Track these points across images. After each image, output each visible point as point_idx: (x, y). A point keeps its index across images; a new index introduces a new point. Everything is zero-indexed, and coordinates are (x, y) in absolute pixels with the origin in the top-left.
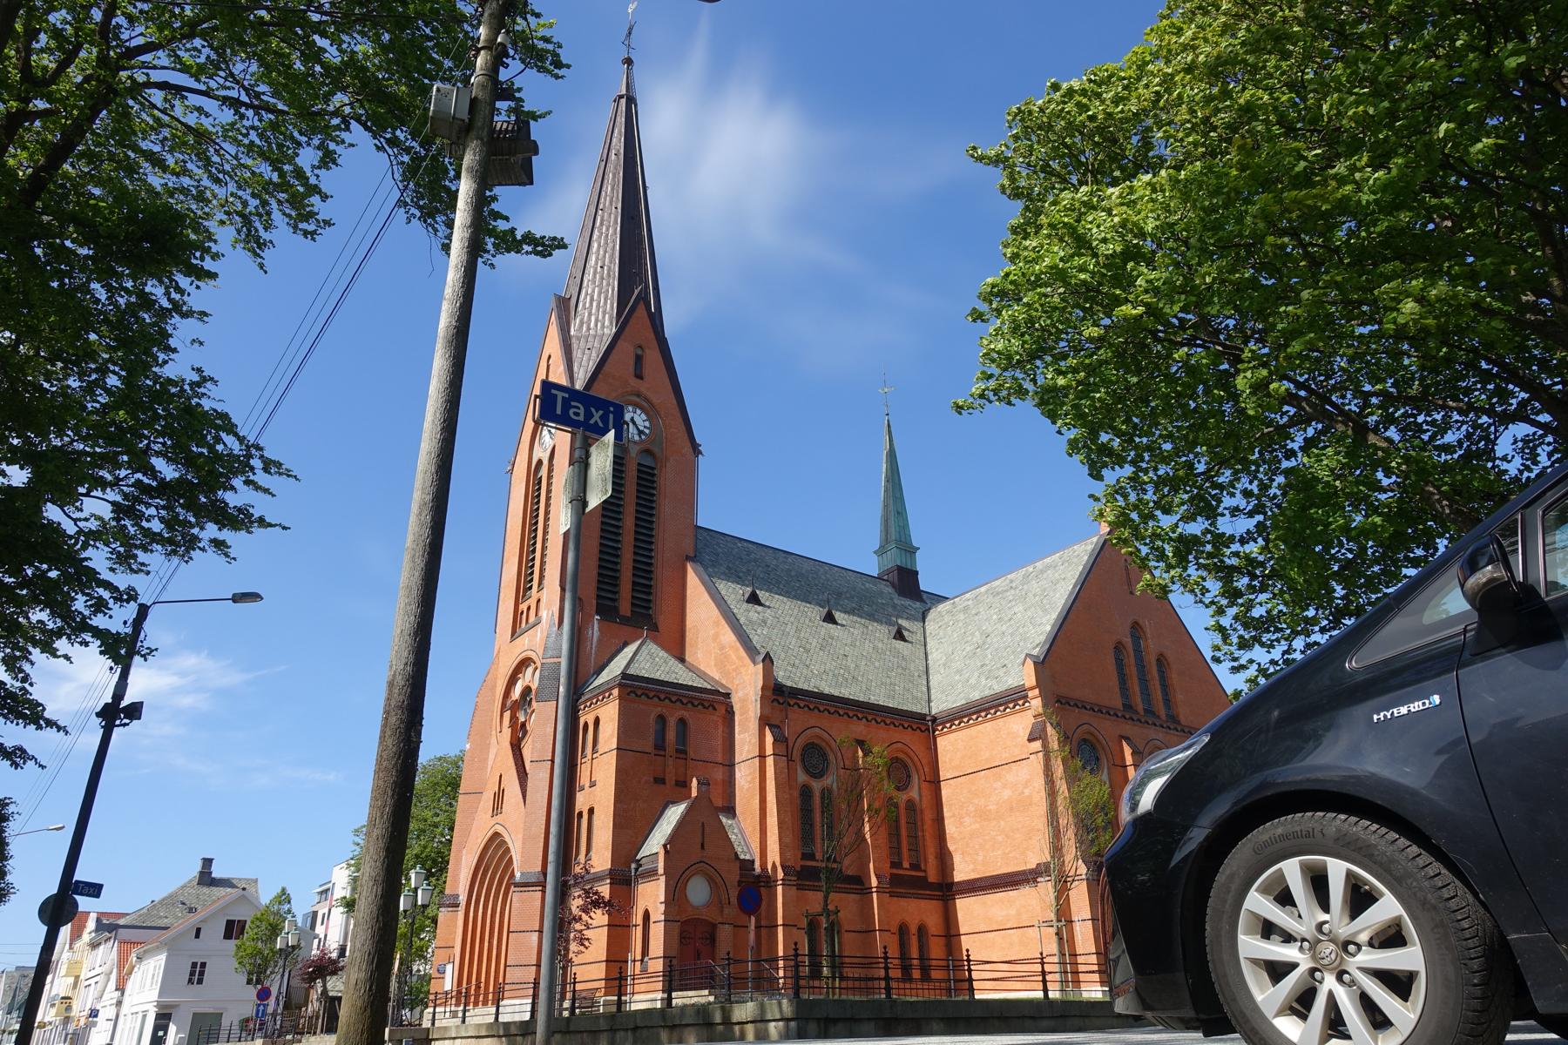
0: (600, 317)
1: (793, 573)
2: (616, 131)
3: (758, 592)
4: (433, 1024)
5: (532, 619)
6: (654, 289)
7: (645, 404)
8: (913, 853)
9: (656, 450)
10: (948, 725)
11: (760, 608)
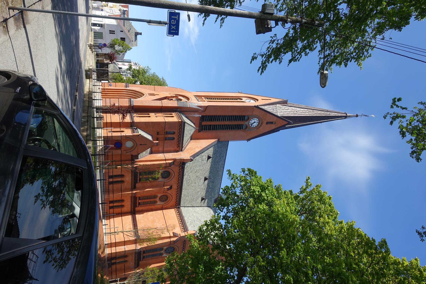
0: (282, 112)
1: (218, 169)
2: (336, 113)
3: (211, 159)
4: (93, 79)
5: (200, 100)
6: (293, 126)
7: (260, 125)
8: (143, 203)
9: (247, 129)
10: (177, 211)
11: (207, 159)
